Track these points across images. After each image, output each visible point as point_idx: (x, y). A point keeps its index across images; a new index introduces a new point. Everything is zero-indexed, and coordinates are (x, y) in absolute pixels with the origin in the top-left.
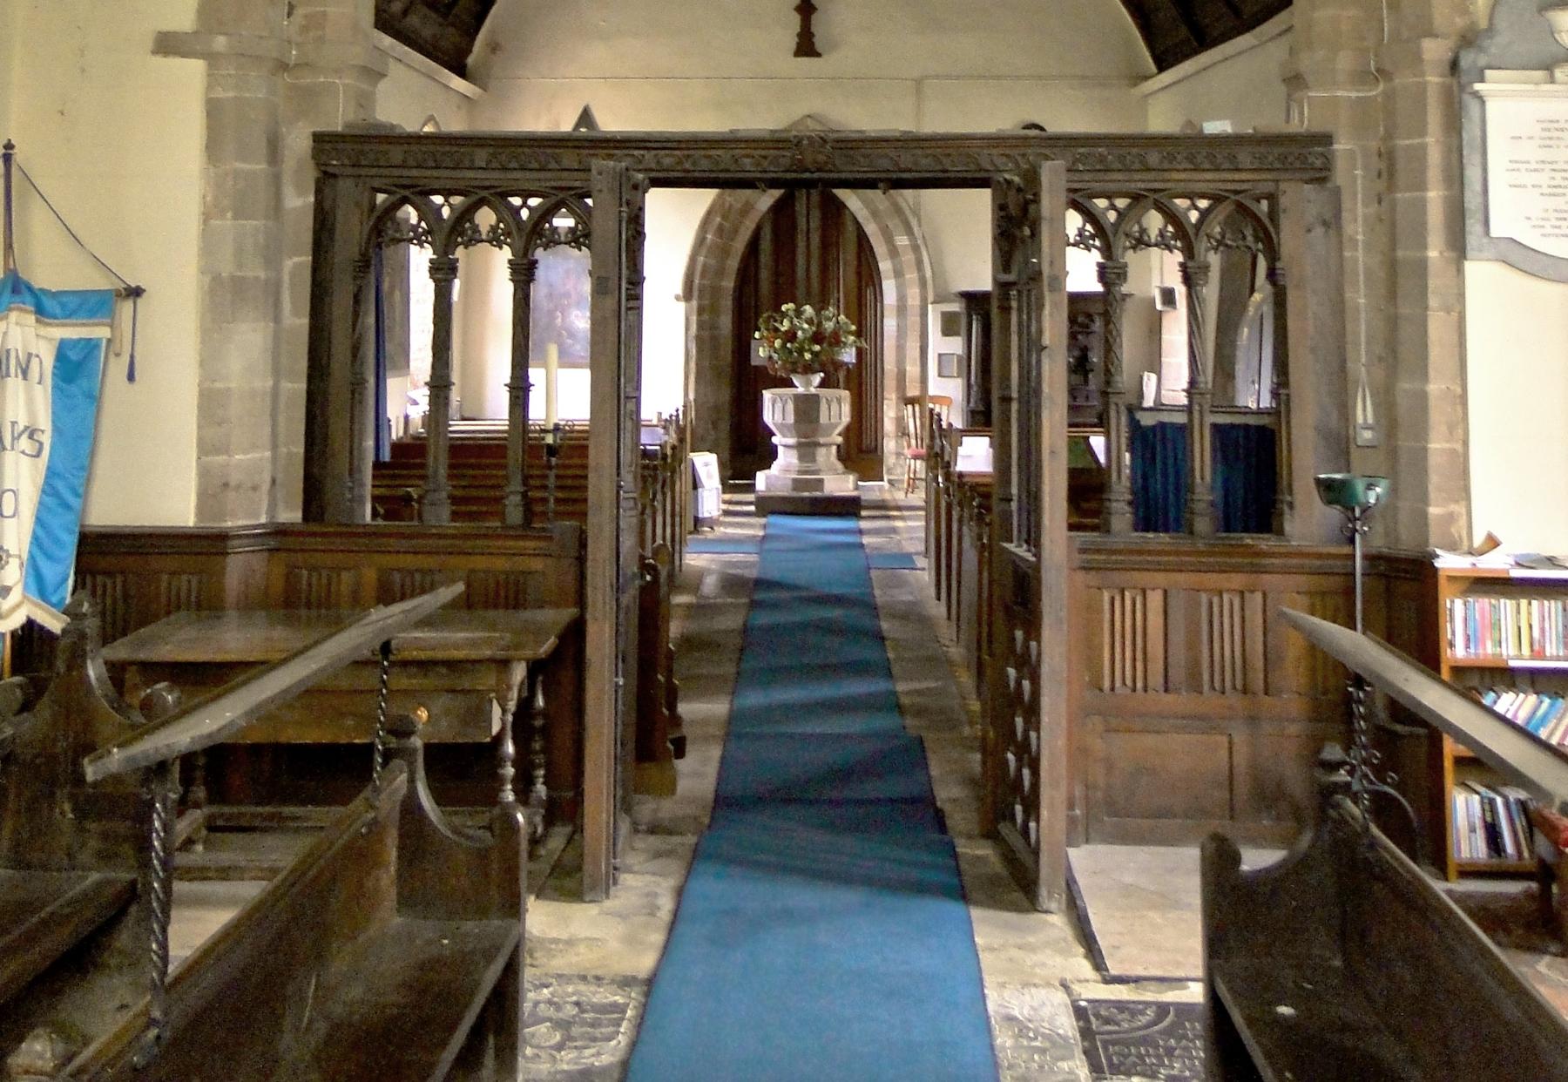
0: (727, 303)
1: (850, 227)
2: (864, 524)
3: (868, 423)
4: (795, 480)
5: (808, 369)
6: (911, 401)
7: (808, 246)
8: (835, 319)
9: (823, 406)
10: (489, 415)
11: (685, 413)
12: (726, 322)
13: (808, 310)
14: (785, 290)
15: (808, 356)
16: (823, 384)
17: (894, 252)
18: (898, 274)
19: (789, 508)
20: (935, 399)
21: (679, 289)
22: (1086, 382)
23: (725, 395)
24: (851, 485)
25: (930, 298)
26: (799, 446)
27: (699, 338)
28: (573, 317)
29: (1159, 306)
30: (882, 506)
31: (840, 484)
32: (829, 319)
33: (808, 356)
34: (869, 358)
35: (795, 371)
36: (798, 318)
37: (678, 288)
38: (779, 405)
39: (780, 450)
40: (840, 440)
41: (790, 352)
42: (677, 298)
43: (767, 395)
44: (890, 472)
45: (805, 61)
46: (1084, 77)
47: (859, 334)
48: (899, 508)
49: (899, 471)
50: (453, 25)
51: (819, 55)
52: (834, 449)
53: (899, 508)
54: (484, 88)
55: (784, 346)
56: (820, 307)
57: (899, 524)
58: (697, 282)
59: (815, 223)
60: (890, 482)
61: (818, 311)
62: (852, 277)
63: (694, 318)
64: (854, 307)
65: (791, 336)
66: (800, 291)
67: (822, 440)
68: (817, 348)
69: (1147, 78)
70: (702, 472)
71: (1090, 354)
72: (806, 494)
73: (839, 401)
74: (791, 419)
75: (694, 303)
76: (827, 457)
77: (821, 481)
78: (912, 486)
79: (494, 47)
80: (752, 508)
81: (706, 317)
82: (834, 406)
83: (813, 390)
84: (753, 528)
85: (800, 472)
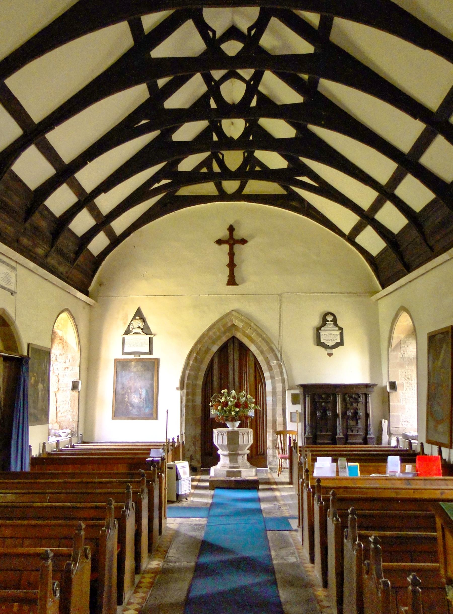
0: (199, 391)
1: (252, 358)
2: (261, 494)
3: (260, 443)
4: (228, 472)
5: (233, 420)
6: (279, 433)
7: (234, 366)
8: (246, 396)
9: (241, 437)
10: (96, 440)
11: (178, 439)
12: (199, 399)
13: (234, 392)
14: (224, 384)
15: (233, 413)
16: (240, 426)
17: (270, 368)
18: (272, 378)
19: (225, 486)
20: (290, 432)
21: (178, 384)
22: (357, 423)
23: (199, 431)
24: (254, 474)
25: (287, 388)
26: (229, 455)
27: (187, 406)
28: (132, 397)
29: (388, 390)
30: (268, 482)
31: (249, 473)
32: (243, 397)
33: (233, 413)
34: (260, 414)
35: (227, 420)
36: (230, 396)
37: (177, 383)
38: (220, 436)
39: (221, 456)
40: (248, 452)
41: (225, 411)
42: (177, 389)
43: (215, 431)
44: (270, 463)
45: (231, 287)
46: (350, 293)
47: (256, 403)
48: (276, 483)
49: (274, 463)
50: (76, 268)
51: (237, 285)
52: (246, 456)
53: (276, 483)
54: (96, 301)
55: (222, 408)
56: (240, 389)
57: (277, 494)
58: (186, 381)
59: (237, 356)
60: (270, 468)
61: (238, 394)
62: (252, 379)
63: (184, 398)
64: (253, 389)
65: (225, 404)
66: (230, 386)
67: (240, 452)
68: (237, 409)
69: (377, 292)
70: (181, 471)
71: (359, 411)
72: (233, 479)
73: (248, 434)
74: (225, 443)
75: (185, 391)
76: (243, 460)
77: (240, 472)
78: (281, 469)
79: (101, 284)
80: (207, 484)
81: (190, 397)
82: (246, 437)
83: (236, 429)
84: (205, 498)
85: (230, 468)
